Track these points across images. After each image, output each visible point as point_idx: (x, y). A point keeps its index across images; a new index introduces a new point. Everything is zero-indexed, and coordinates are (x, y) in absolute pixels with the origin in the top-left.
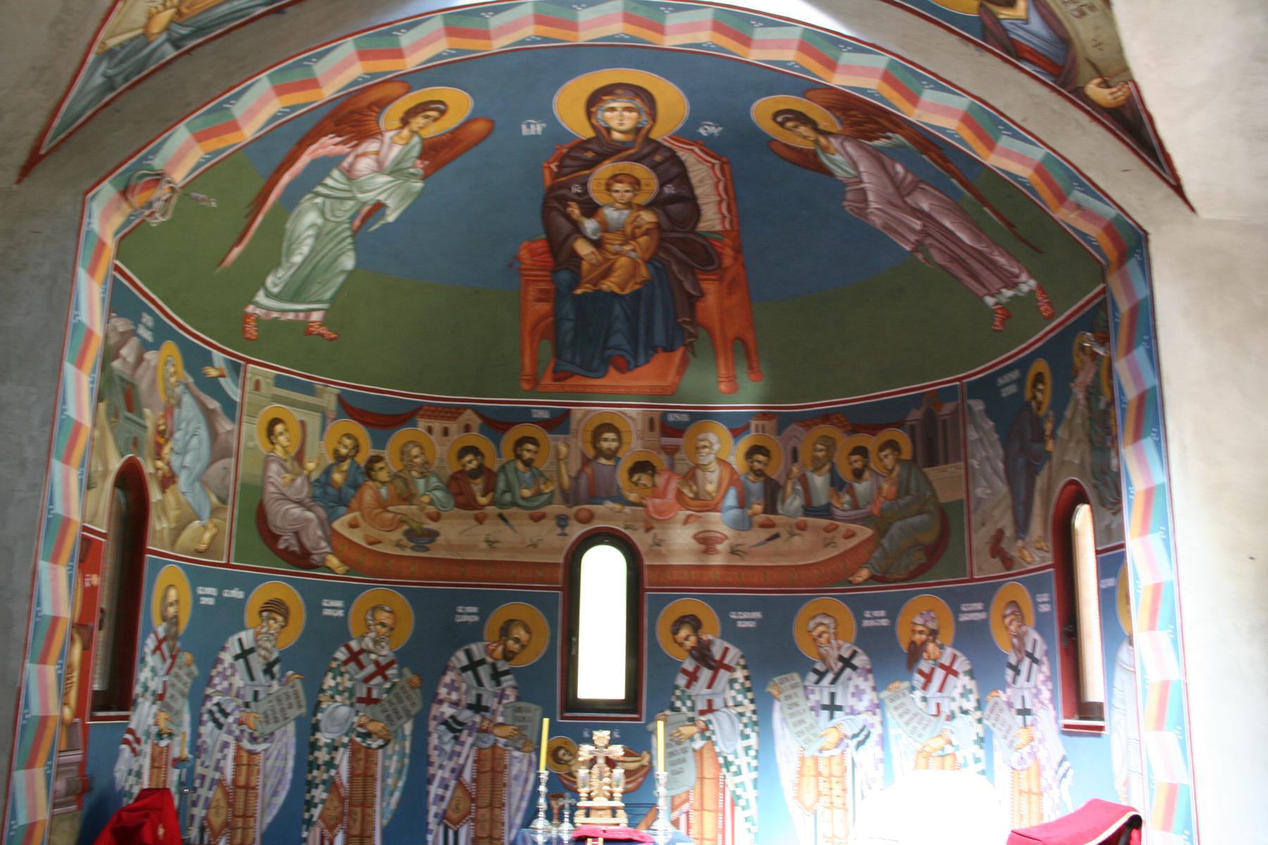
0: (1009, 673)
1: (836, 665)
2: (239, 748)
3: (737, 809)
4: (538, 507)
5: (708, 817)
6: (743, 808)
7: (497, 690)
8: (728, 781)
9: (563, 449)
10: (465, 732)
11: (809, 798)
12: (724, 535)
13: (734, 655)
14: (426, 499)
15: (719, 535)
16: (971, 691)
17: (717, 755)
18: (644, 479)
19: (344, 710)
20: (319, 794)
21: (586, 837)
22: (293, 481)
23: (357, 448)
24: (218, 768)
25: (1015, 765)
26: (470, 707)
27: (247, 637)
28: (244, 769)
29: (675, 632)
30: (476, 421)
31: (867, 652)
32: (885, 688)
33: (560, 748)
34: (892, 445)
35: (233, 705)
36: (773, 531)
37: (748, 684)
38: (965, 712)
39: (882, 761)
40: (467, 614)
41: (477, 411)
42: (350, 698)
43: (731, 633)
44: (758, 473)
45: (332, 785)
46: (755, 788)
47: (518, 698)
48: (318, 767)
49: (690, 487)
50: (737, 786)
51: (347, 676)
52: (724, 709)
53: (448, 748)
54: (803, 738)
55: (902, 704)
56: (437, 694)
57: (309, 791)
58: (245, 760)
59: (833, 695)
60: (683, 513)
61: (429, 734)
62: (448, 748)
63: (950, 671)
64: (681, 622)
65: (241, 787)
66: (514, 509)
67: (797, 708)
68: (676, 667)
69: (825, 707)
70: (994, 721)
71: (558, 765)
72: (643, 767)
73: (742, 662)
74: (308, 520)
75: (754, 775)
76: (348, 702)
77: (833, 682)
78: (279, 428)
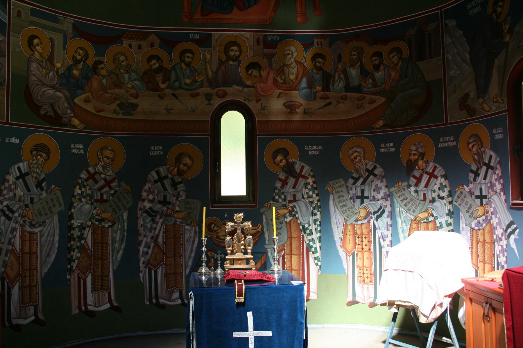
0: (471, 176)
1: (365, 174)
2: (23, 231)
3: (311, 253)
4: (194, 89)
5: (294, 258)
6: (313, 253)
7: (176, 193)
8: (305, 239)
9: (208, 56)
10: (158, 216)
11: (350, 246)
12: (301, 104)
13: (307, 169)
14: (129, 86)
15: (298, 104)
16: (445, 186)
17: (299, 225)
18: (255, 73)
19: (87, 207)
20: (76, 254)
21: (234, 280)
22: (47, 74)
23: (87, 55)
24: (10, 243)
25: (473, 226)
26: (160, 202)
27: (23, 166)
28: (28, 243)
29: (274, 158)
30: (157, 41)
31: (382, 166)
32: (394, 186)
33: (212, 223)
34: (398, 50)
35: (17, 206)
36: (328, 101)
37: (315, 186)
38: (442, 198)
39: (391, 226)
40: (157, 151)
41: (157, 35)
42: (91, 200)
43: (305, 157)
44: (319, 69)
45: (83, 249)
46: (320, 242)
47: (187, 197)
48: (74, 239)
49: (281, 77)
50: (310, 241)
51: (88, 188)
52: (302, 200)
53: (149, 226)
54: (346, 214)
55: (403, 194)
56: (141, 196)
57: (69, 253)
58: (28, 238)
59: (363, 191)
60: (277, 92)
61: (138, 218)
62: (149, 226)
63: (432, 175)
64: (277, 152)
65: (27, 253)
66: (181, 91)
67: (343, 198)
68: (276, 177)
69: (358, 197)
70: (460, 203)
71: (211, 233)
72: (258, 232)
73: (311, 174)
74: (59, 98)
75: (318, 235)
76: (90, 202)
77: (363, 183)
78: (36, 41)
